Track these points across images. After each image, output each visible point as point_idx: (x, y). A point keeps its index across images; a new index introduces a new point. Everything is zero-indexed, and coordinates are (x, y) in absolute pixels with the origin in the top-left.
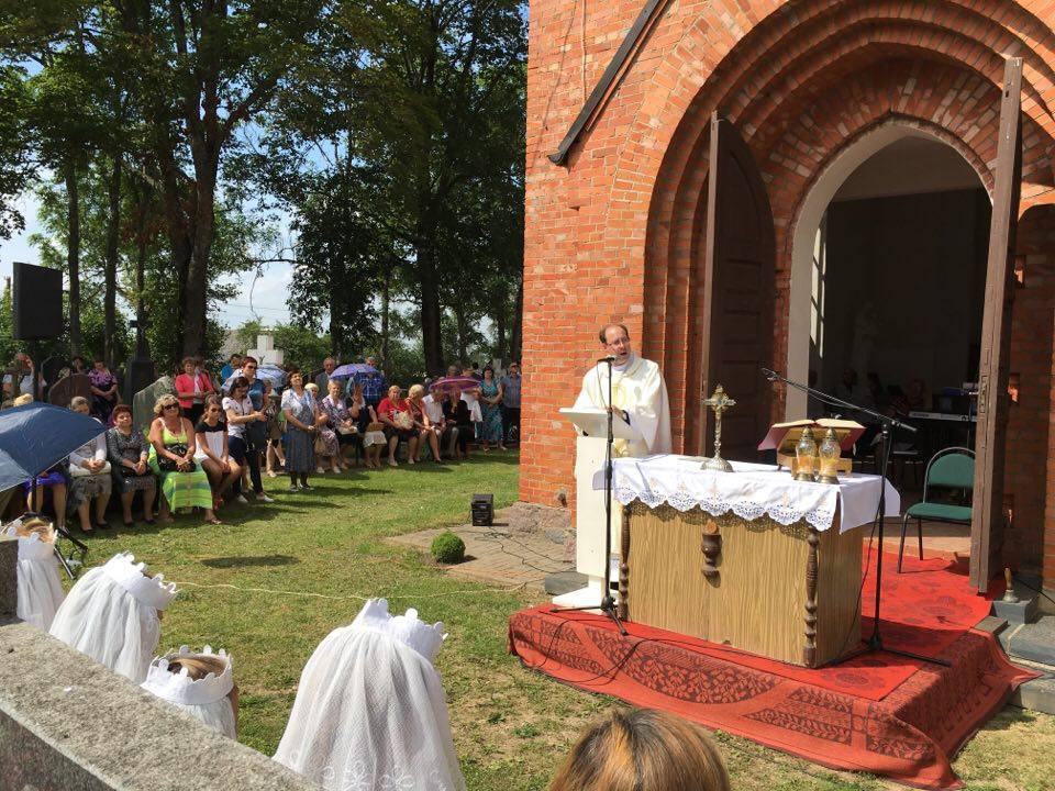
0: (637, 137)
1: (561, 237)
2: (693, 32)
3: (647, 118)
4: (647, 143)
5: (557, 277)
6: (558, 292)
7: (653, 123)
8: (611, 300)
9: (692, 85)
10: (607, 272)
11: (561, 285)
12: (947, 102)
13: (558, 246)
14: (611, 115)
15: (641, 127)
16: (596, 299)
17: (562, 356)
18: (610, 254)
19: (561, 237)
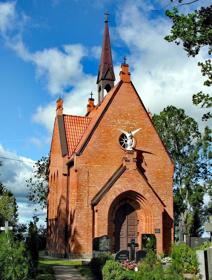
0: (107, 203)
1: (83, 212)
2: (114, 192)
3: (108, 201)
4: (108, 204)
6: (83, 220)
7: (109, 201)
10: (102, 219)
11: (83, 219)
13: (82, 213)
14: (102, 200)
16: (101, 223)
19: (83, 212)
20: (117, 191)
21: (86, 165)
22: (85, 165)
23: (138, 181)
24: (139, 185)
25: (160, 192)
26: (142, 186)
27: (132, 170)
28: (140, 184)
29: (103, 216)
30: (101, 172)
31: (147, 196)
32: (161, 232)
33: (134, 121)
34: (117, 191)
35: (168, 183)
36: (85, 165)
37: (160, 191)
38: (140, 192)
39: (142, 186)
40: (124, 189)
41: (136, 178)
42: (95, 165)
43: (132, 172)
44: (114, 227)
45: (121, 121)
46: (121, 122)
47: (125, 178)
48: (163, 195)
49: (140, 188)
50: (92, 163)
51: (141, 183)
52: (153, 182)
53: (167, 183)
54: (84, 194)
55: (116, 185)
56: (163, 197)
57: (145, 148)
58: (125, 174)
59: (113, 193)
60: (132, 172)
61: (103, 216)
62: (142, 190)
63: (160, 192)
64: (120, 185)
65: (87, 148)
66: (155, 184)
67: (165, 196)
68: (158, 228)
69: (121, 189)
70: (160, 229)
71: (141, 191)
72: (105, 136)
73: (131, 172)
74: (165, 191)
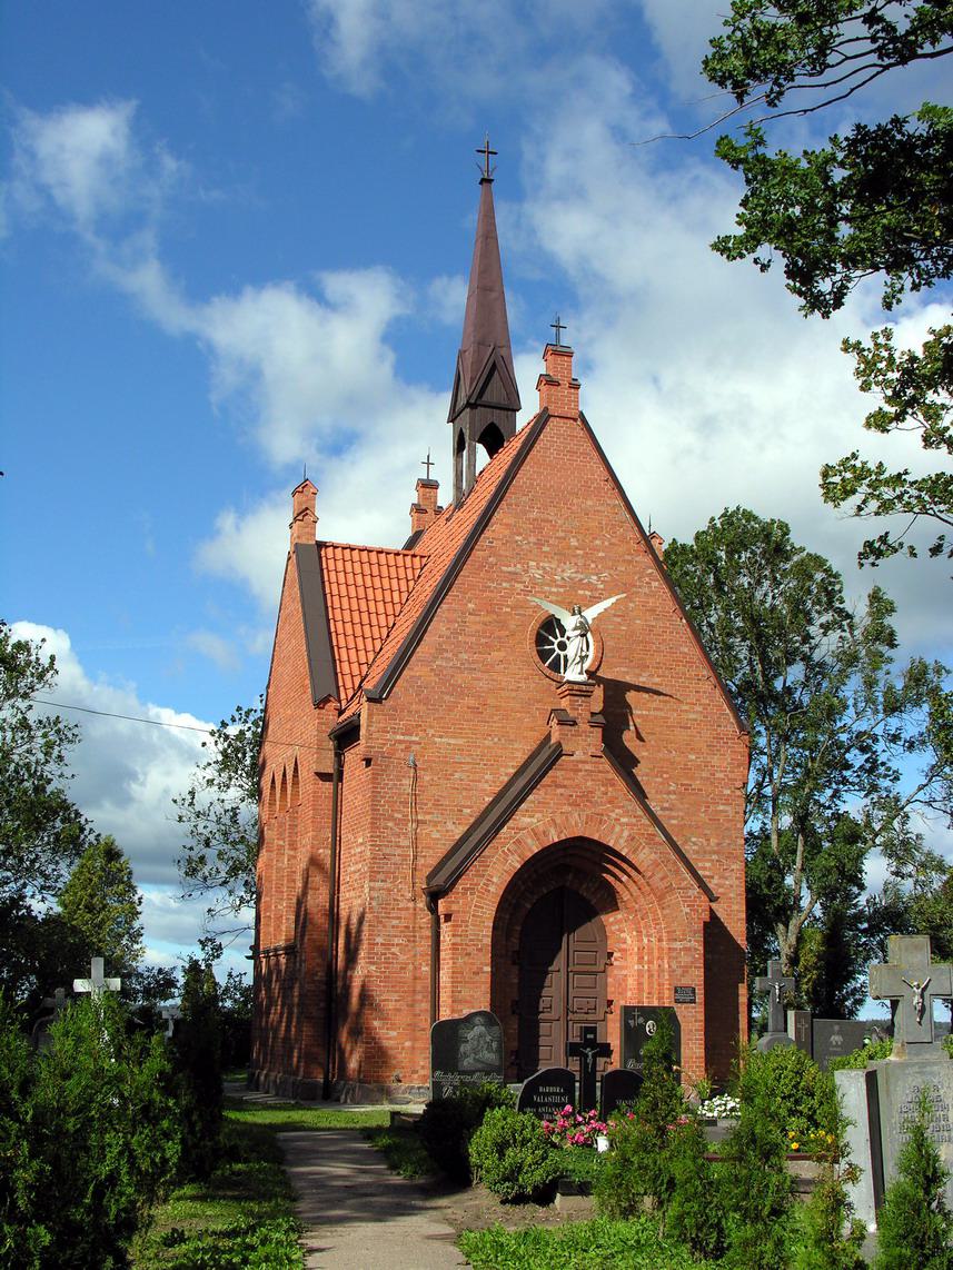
1: (395, 922)
4: (492, 889)
5: (393, 945)
6: (393, 954)
7: (495, 880)
8: (473, 964)
9: (514, 867)
10: (469, 949)
12: (584, 886)
13: (393, 927)
15: (488, 880)
16: (465, 963)
17: (396, 992)
18: (472, 940)
19: (395, 922)
20: (529, 841)
21: (407, 738)
22: (402, 737)
23: (610, 802)
24: (613, 815)
25: (695, 844)
26: (623, 820)
27: (583, 757)
28: (617, 811)
29: (475, 935)
30: (466, 767)
31: (644, 857)
32: (700, 997)
33: (593, 566)
34: (529, 841)
35: (727, 808)
36: (402, 737)
37: (693, 839)
38: (616, 842)
39: (623, 820)
40: (553, 831)
41: (603, 789)
42: (441, 737)
43: (587, 767)
44: (516, 981)
45: (544, 568)
46: (541, 572)
47: (559, 791)
48: (707, 857)
49: (618, 829)
50: (431, 732)
51: (619, 807)
52: (666, 805)
53: (721, 808)
54: (398, 851)
55: (524, 816)
56: (708, 865)
57: (637, 671)
58: (559, 773)
59: (513, 848)
60: (587, 767)
61: (475, 935)
62: (626, 834)
63: (695, 844)
64: (538, 815)
65: (412, 673)
66: (674, 814)
67: (715, 857)
68: (685, 981)
69: (544, 832)
70: (694, 989)
71: (622, 841)
72: (479, 627)
73: (580, 766)
74: (713, 841)
